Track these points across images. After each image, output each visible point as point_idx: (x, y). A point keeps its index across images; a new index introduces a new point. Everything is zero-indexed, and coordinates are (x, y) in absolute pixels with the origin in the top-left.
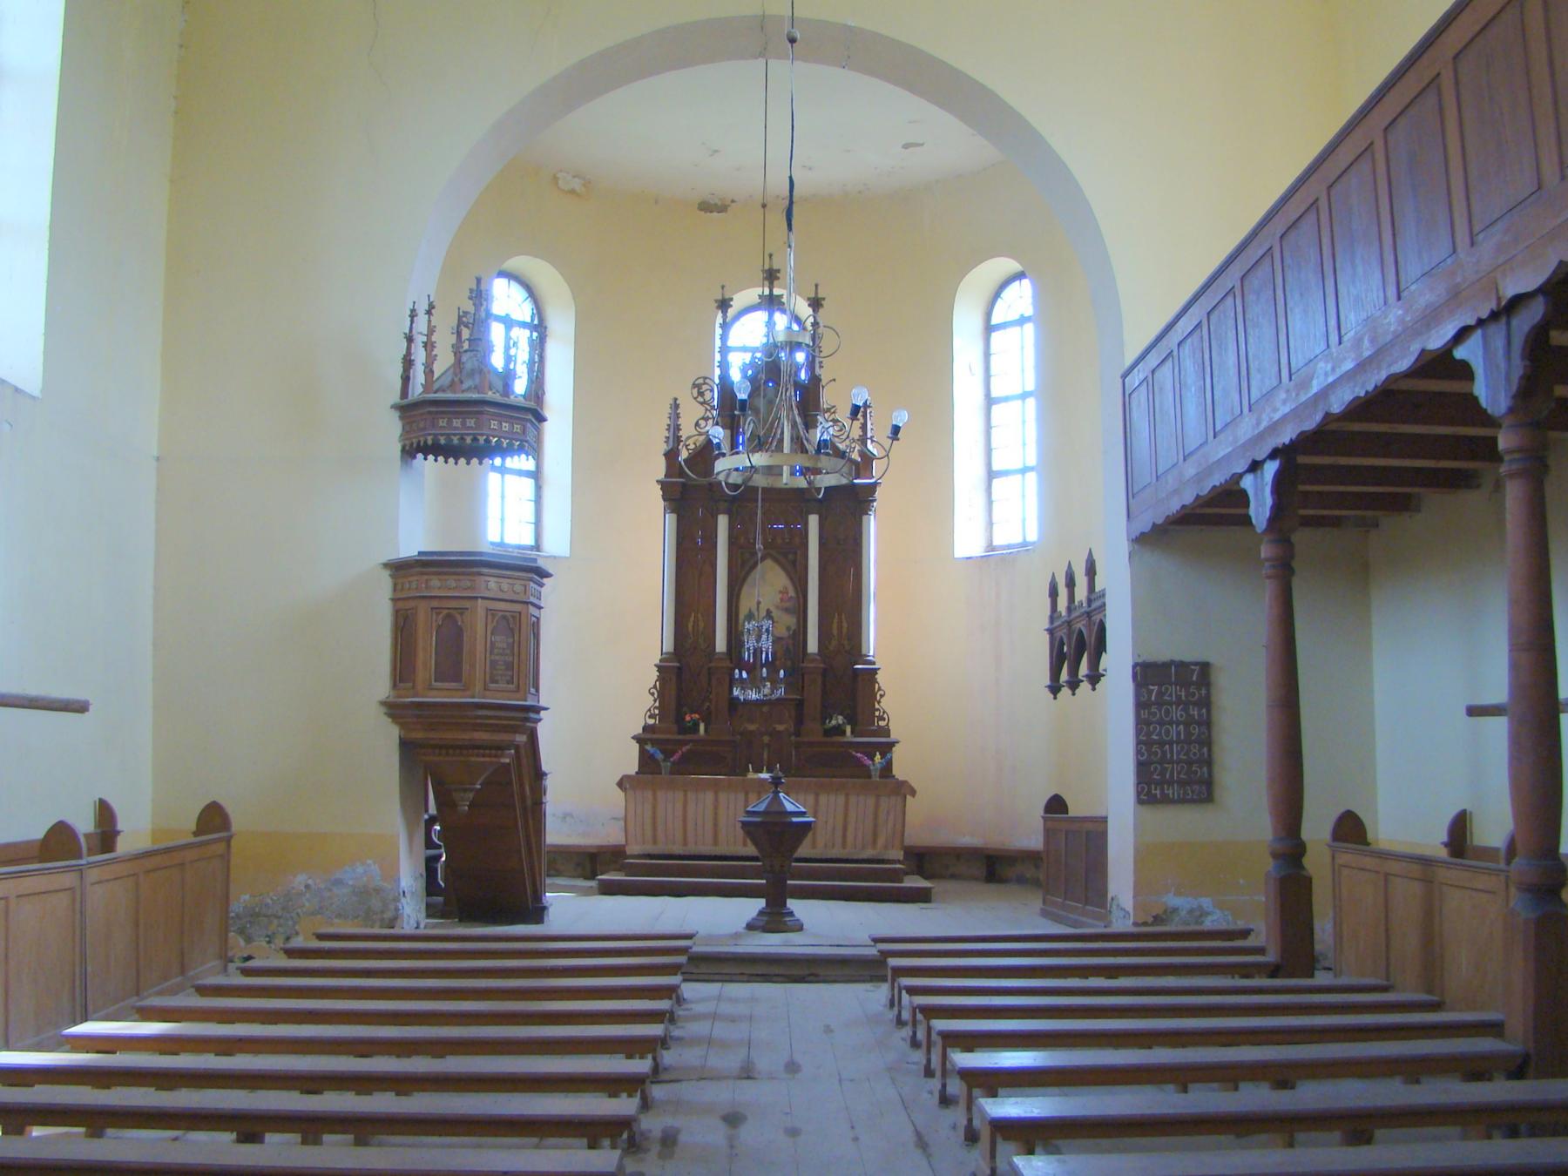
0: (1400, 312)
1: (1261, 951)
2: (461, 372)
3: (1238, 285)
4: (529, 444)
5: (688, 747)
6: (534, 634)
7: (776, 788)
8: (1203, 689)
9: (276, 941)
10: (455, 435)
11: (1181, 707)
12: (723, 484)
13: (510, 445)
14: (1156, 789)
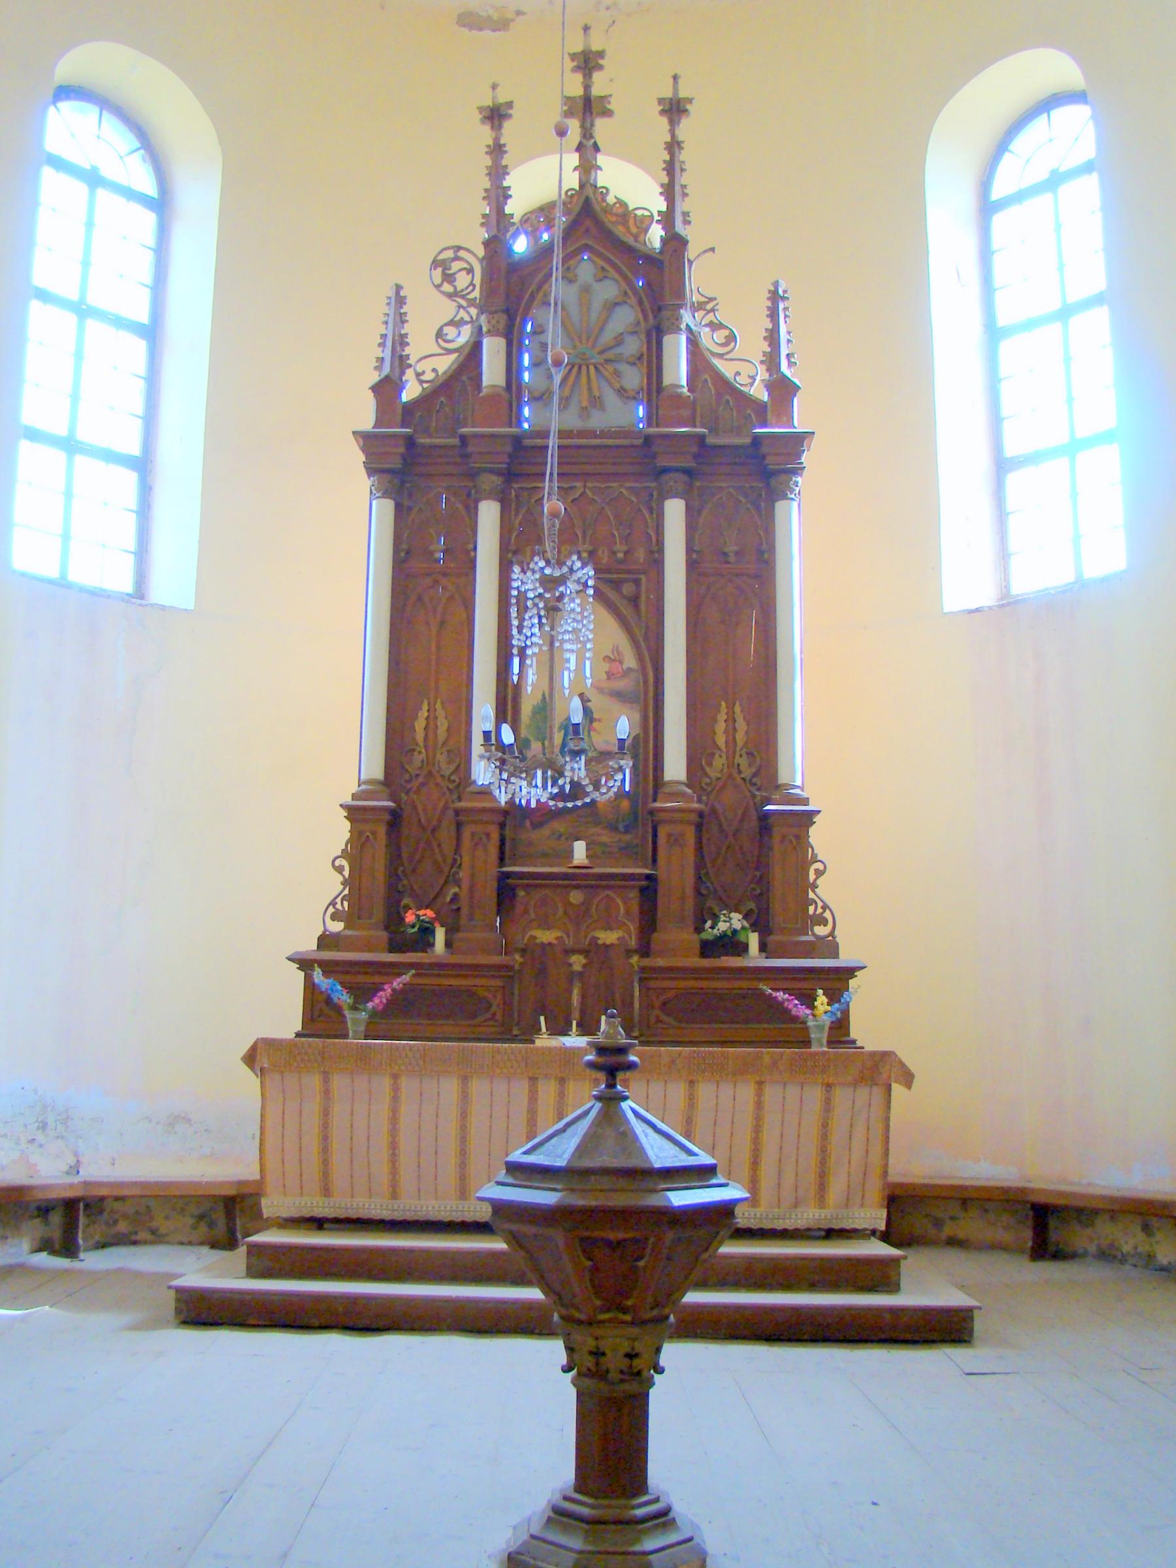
5: (406, 978)
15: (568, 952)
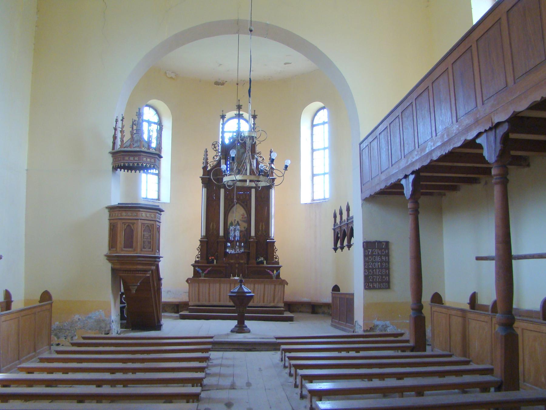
0: (457, 126)
1: (407, 341)
2: (133, 141)
3: (400, 115)
4: (157, 166)
5: (210, 268)
6: (158, 231)
7: (241, 283)
8: (387, 250)
9: (68, 338)
10: (131, 163)
11: (379, 256)
12: (226, 185)
13: (150, 166)
14: (371, 285)
15: (235, 264)
